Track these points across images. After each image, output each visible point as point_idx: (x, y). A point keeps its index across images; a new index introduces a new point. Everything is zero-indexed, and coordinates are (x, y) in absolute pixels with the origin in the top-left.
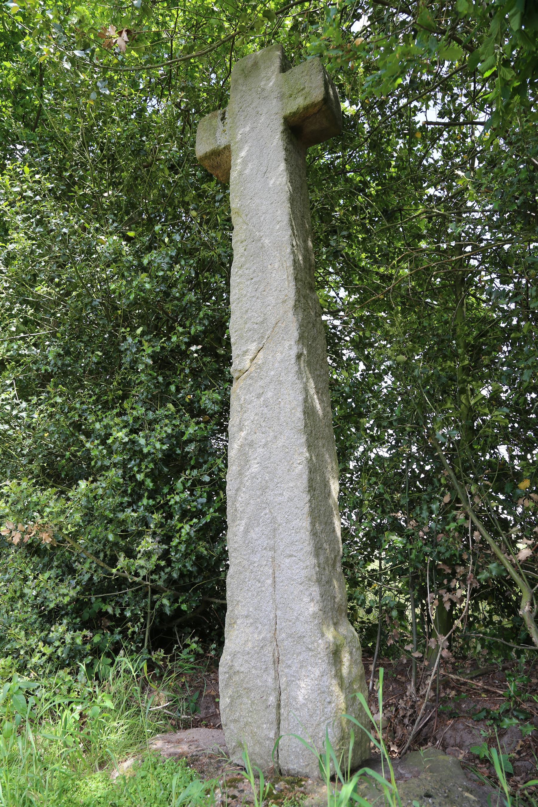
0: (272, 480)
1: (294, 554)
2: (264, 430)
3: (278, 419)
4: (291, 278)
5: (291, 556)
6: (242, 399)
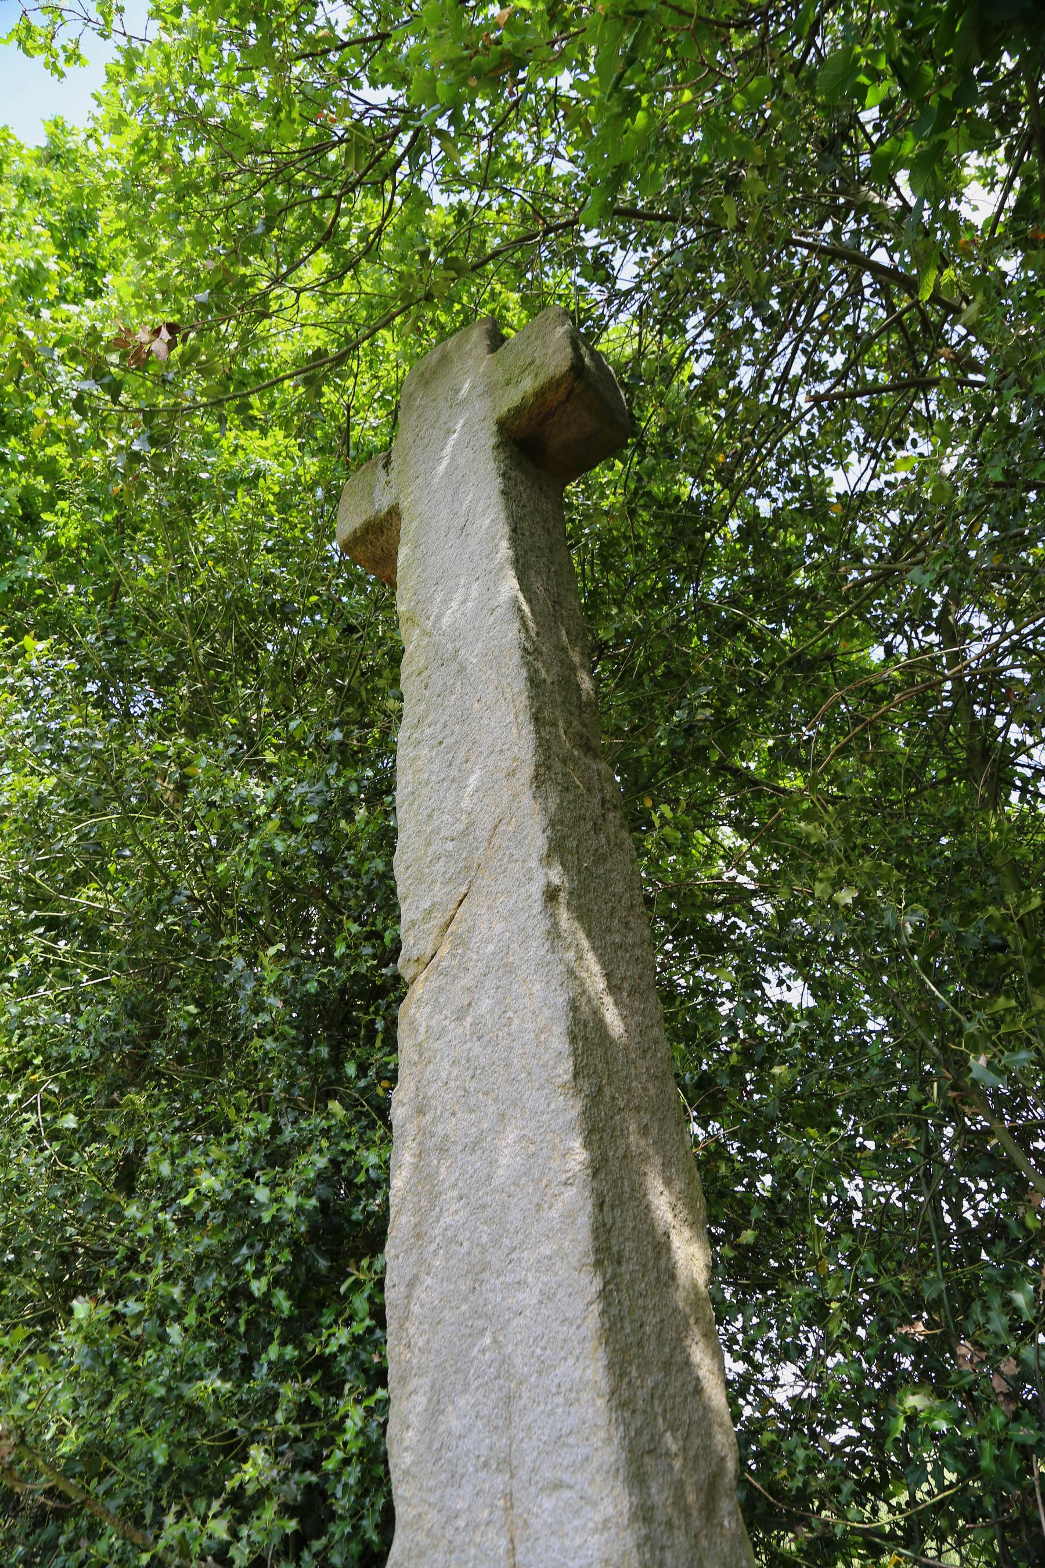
0: (496, 1242)
1: (566, 1477)
2: (473, 1101)
3: (508, 1066)
4: (525, 718)
5: (558, 1486)
6: (422, 1030)
